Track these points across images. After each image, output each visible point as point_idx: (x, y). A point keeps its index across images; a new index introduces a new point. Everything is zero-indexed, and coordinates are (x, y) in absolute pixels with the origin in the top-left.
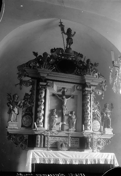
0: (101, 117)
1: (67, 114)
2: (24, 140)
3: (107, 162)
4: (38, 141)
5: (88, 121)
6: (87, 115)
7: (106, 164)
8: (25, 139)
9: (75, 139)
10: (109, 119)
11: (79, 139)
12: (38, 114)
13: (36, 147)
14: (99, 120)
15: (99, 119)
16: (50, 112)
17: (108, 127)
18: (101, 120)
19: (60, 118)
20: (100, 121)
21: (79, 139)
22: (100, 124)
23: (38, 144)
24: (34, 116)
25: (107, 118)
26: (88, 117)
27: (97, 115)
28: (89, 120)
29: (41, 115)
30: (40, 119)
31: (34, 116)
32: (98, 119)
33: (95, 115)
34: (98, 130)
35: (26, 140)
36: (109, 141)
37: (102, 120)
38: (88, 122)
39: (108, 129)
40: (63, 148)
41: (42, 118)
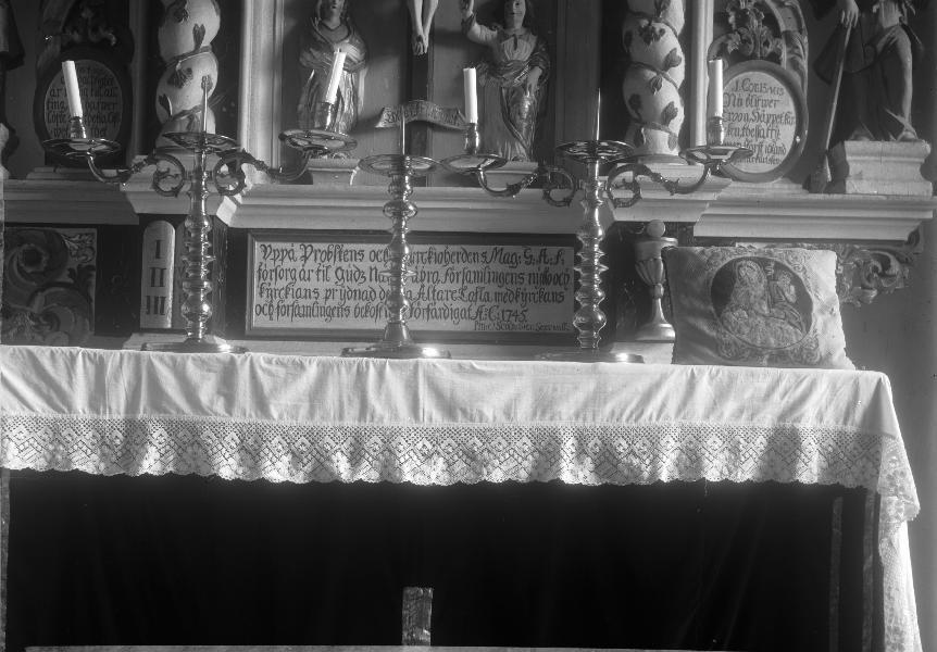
0: (803, 43)
1: (453, 24)
2: (65, 278)
3: (209, 459)
4: (158, 277)
5: (651, 74)
6: (642, 15)
7: (194, 479)
8: (73, 263)
9: (535, 251)
10: (892, 50)
11: (94, 231)
12: (162, 34)
13: (142, 331)
14: (785, 64)
15: (784, 56)
16: (292, 23)
17: (884, 129)
18: (804, 63)
19: (389, 71)
20: (796, 77)
21: (94, 231)
22: (791, 108)
23: (158, 307)
24: (137, 66)
25: (872, 42)
26: (650, 36)
27: (770, 21)
28: (670, 62)
29: (188, 43)
30: (179, 80)
31: (137, 66)
32: (775, 57)
33: (743, 19)
34: (767, 167)
35: (80, 275)
36: (886, 264)
37: (822, 68)
38: (656, 85)
39: (879, 145)
40: (735, 316)
41: (206, 70)
